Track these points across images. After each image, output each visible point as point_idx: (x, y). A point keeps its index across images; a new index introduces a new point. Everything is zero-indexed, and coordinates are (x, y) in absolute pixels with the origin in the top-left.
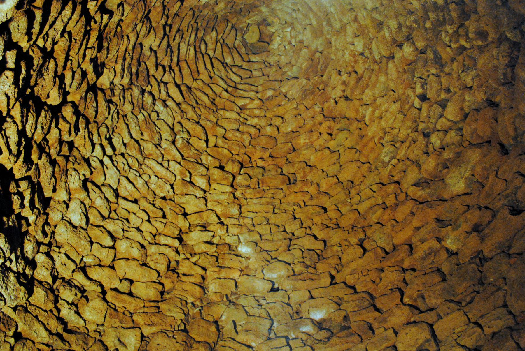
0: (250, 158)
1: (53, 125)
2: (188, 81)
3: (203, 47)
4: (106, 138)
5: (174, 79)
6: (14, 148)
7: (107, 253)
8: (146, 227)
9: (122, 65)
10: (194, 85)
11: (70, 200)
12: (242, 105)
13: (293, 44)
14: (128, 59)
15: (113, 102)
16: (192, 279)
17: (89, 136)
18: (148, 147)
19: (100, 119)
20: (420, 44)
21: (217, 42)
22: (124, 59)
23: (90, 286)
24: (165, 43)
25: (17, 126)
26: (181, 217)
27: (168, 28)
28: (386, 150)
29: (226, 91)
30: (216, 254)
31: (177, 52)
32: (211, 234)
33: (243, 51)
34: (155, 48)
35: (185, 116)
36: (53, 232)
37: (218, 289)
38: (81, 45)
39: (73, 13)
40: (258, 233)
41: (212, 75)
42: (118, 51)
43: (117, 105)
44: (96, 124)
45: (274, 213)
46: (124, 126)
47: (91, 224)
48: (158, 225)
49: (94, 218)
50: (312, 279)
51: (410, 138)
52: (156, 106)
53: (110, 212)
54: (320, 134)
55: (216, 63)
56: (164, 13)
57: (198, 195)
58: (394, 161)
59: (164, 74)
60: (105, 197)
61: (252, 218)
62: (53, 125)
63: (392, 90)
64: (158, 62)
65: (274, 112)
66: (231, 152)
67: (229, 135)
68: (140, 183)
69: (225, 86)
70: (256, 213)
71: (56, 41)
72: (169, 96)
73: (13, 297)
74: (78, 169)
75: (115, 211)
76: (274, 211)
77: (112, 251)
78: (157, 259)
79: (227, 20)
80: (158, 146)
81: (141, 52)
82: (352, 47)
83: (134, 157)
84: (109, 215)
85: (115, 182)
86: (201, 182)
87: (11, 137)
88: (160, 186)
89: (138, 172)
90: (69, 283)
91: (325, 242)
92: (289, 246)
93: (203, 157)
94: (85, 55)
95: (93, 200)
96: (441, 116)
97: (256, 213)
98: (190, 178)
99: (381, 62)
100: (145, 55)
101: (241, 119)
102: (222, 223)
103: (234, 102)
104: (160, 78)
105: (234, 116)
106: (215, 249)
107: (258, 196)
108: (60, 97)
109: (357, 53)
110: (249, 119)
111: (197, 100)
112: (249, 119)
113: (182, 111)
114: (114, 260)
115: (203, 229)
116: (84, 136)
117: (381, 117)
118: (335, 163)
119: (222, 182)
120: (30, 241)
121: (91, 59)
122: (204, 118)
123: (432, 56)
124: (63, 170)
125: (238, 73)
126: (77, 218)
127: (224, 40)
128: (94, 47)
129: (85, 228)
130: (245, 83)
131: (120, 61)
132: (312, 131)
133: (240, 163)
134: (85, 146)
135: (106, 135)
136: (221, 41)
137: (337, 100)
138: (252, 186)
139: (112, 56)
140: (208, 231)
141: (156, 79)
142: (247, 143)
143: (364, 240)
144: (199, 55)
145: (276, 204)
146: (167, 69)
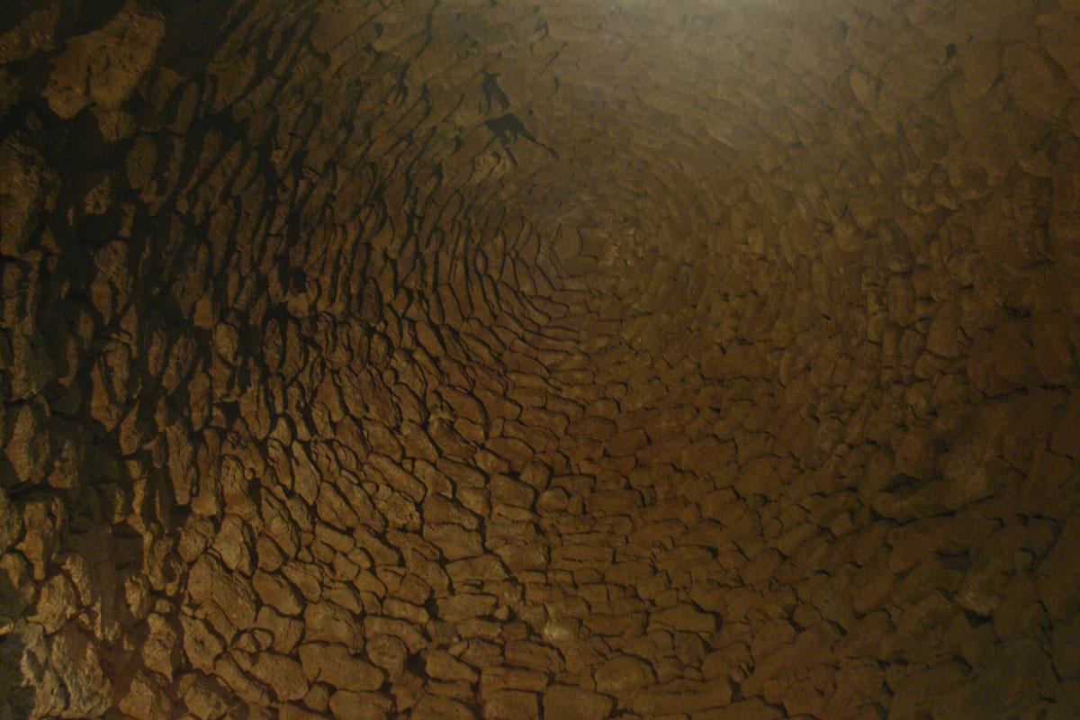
0: (567, 458)
1: (199, 367)
2: (453, 320)
3: (480, 262)
4: (298, 407)
5: (428, 314)
6: (121, 393)
7: (287, 627)
8: (365, 582)
9: (332, 278)
10: (465, 328)
11: (223, 515)
12: (552, 364)
13: (640, 254)
14: (344, 269)
15: (315, 343)
16: (452, 691)
17: (266, 400)
18: (377, 432)
19: (289, 370)
20: (865, 220)
21: (505, 256)
22: (337, 268)
23: (246, 692)
24: (411, 246)
25: (130, 351)
26: (433, 567)
27: (416, 223)
28: (823, 428)
29: (523, 339)
30: (499, 641)
31: (433, 267)
32: (491, 601)
33: (552, 272)
34: (392, 255)
35: (446, 381)
36: (185, 576)
37: (503, 712)
38: (257, 227)
39: (242, 165)
40: (584, 600)
41: (497, 311)
42: (325, 252)
43: (321, 349)
44: (280, 379)
45: (614, 561)
46: (332, 389)
47: (262, 570)
48: (388, 578)
49: (269, 560)
50: (695, 692)
51: (867, 401)
52: (393, 360)
53: (299, 549)
54: (698, 410)
55: (503, 291)
56: (408, 192)
57: (466, 524)
58: (841, 448)
59: (409, 305)
60: (291, 519)
61: (572, 573)
62: (199, 367)
63: (825, 316)
64: (400, 279)
65: (610, 374)
66: (530, 448)
67: (527, 417)
68: (358, 496)
69: (520, 331)
70: (580, 561)
71: (211, 208)
72: (419, 344)
73: (85, 694)
74: (241, 457)
75: (308, 547)
76: (614, 558)
77: (297, 624)
78: (384, 646)
79: (523, 218)
80: (395, 432)
81: (368, 259)
82: (743, 247)
83: (350, 449)
84: (297, 554)
85: (310, 491)
86: (473, 501)
87: (116, 369)
88: (395, 506)
89: (355, 475)
90: (207, 680)
91: (716, 615)
92: (645, 625)
93: (479, 456)
94: (263, 248)
95: (267, 522)
96: (922, 350)
97: (580, 561)
98: (454, 492)
99: (798, 268)
100: (374, 265)
101: (550, 390)
102: (513, 581)
103: (536, 359)
104: (402, 311)
105: (537, 382)
106: (500, 630)
107: (582, 529)
108: (213, 314)
109: (753, 258)
110: (564, 388)
111: (470, 353)
112: (564, 388)
113: (441, 372)
114: (298, 644)
115: (475, 590)
116: (258, 398)
117: (808, 368)
118: (728, 463)
119: (517, 502)
120: (137, 584)
121: (275, 256)
122: (481, 386)
123: (889, 239)
124: (213, 455)
125: (544, 310)
126: (232, 554)
127: (517, 254)
128: (282, 236)
129: (249, 573)
130: (558, 327)
131: (329, 271)
132: (681, 406)
133: (546, 465)
134: (257, 417)
135: (299, 402)
136: (513, 255)
137: (724, 346)
138: (570, 511)
139: (315, 260)
140: (488, 594)
141: (395, 313)
142: (560, 432)
143: (795, 607)
144: (473, 276)
145: (619, 545)
146: (416, 295)
